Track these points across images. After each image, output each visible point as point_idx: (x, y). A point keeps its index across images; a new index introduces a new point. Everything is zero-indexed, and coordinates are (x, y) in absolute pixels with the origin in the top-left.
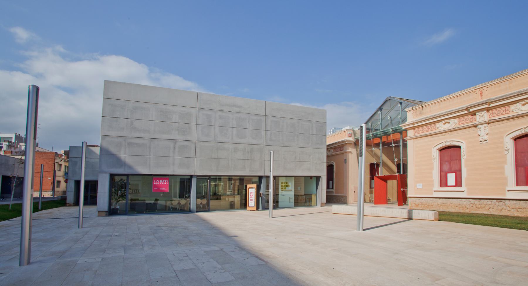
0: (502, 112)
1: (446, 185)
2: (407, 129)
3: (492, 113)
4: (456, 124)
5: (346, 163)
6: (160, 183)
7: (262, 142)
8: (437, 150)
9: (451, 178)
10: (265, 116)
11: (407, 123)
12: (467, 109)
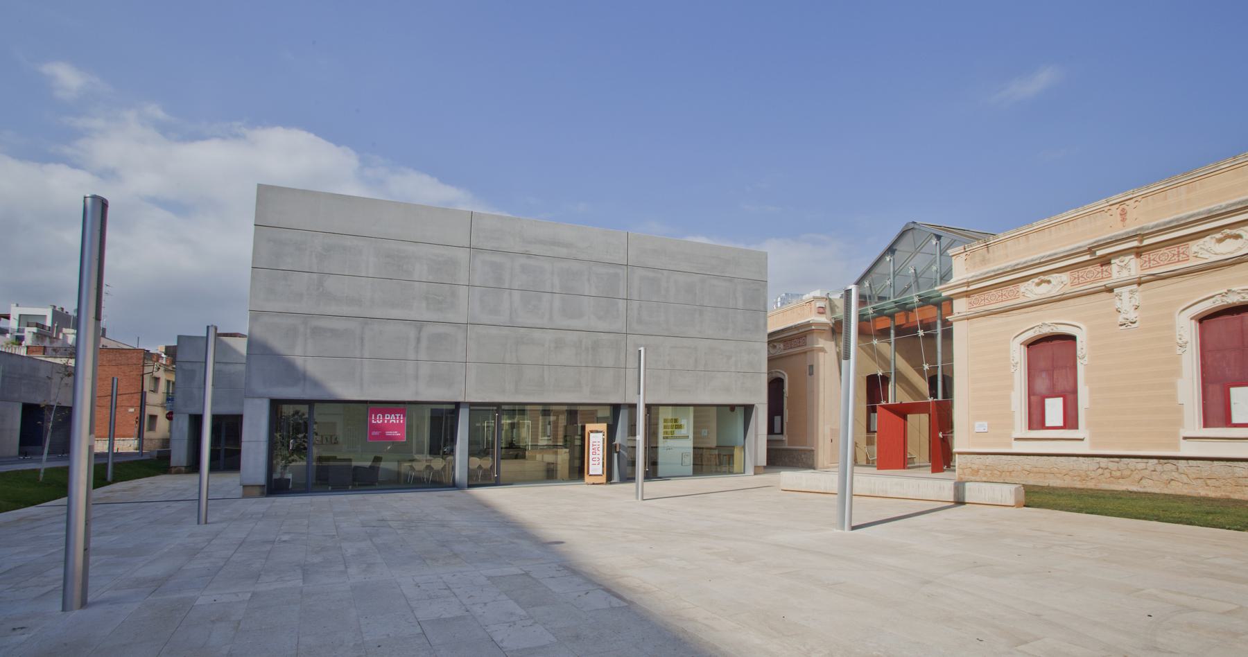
1: (1042, 426)
5: (811, 374)
6: (386, 421)
7: (619, 325)
10: (625, 267)
11: (953, 282)
12: (1091, 250)
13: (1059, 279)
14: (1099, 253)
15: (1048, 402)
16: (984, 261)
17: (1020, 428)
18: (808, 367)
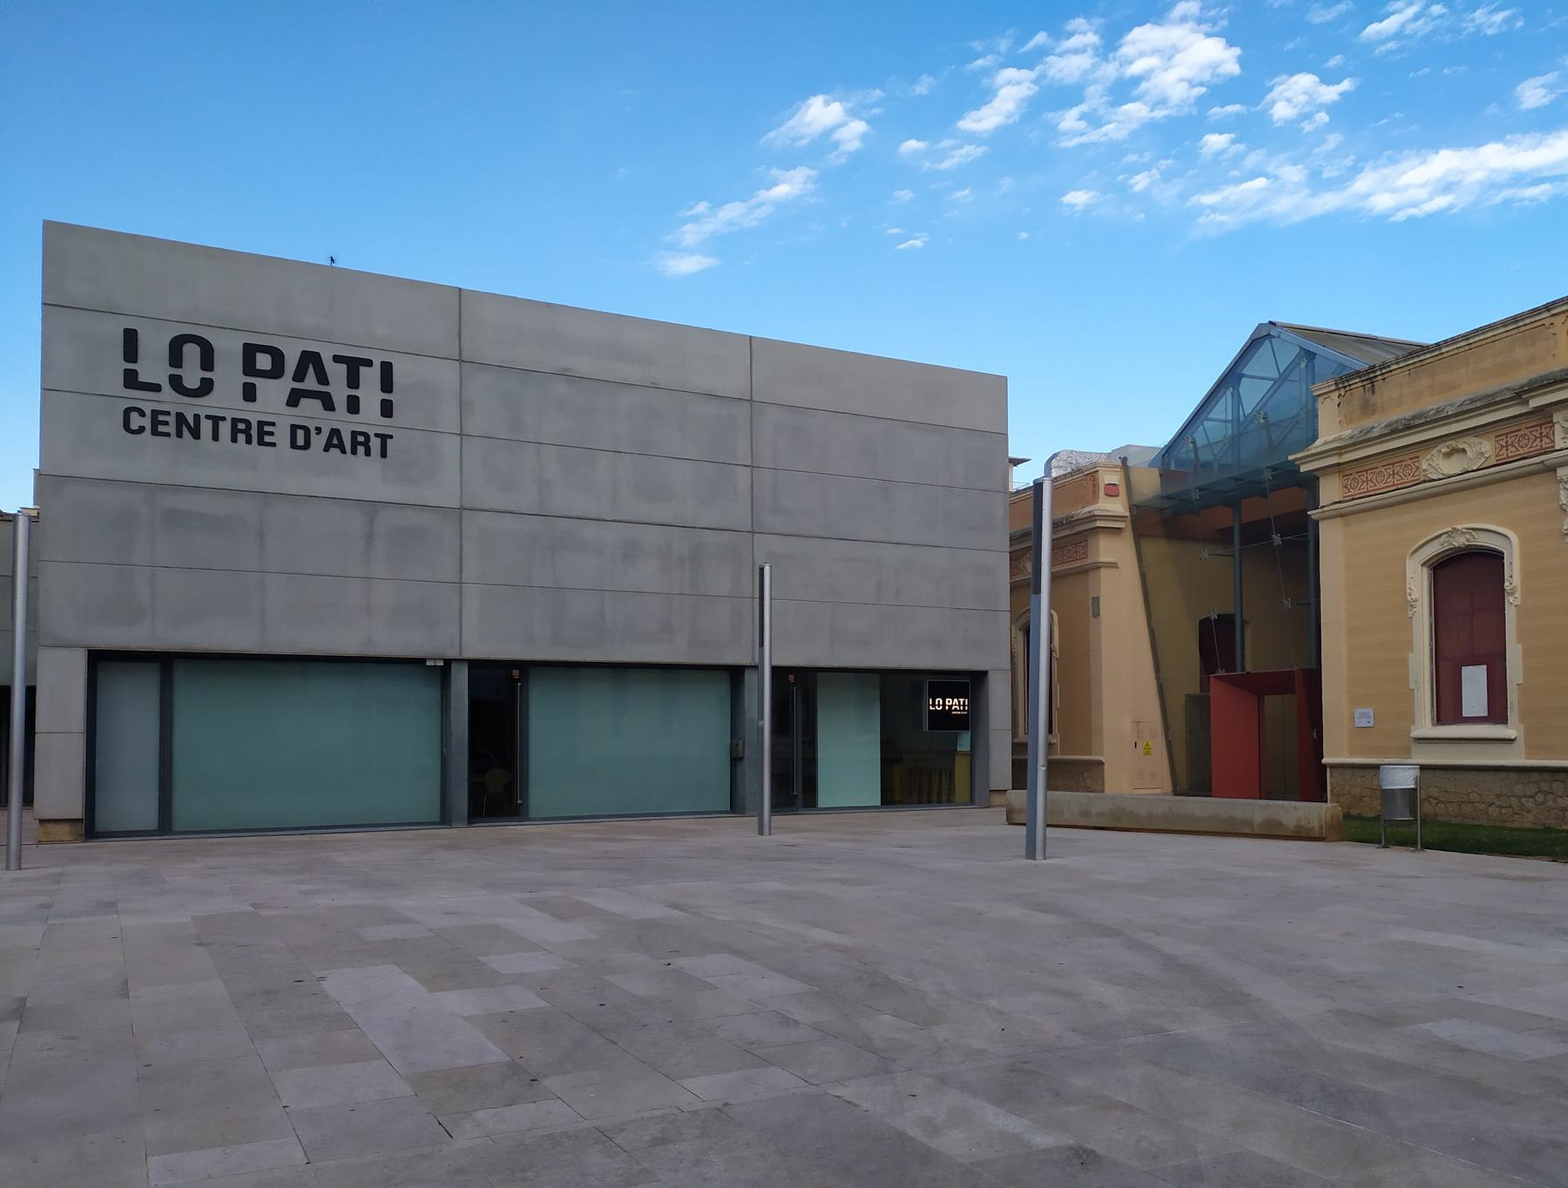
0: (1531, 441)
1: (1458, 718)
2: (1315, 473)
3: (1365, 479)
4: (1487, 458)
5: (1096, 614)
6: (947, 708)
7: (739, 515)
8: (1423, 565)
9: (1474, 681)
10: (748, 404)
11: (1318, 446)
12: (1520, 395)
13: (1477, 448)
14: (1535, 403)
15: (1466, 671)
16: (1367, 408)
17: (1425, 726)
18: (1091, 602)
